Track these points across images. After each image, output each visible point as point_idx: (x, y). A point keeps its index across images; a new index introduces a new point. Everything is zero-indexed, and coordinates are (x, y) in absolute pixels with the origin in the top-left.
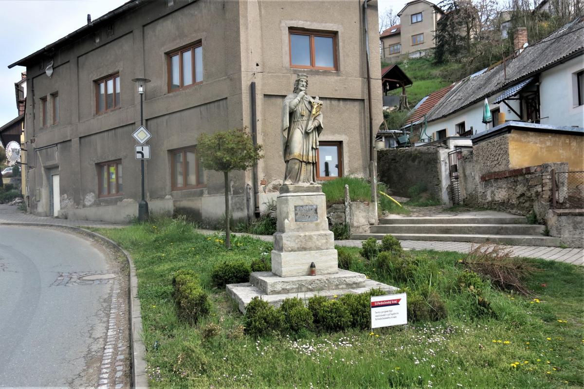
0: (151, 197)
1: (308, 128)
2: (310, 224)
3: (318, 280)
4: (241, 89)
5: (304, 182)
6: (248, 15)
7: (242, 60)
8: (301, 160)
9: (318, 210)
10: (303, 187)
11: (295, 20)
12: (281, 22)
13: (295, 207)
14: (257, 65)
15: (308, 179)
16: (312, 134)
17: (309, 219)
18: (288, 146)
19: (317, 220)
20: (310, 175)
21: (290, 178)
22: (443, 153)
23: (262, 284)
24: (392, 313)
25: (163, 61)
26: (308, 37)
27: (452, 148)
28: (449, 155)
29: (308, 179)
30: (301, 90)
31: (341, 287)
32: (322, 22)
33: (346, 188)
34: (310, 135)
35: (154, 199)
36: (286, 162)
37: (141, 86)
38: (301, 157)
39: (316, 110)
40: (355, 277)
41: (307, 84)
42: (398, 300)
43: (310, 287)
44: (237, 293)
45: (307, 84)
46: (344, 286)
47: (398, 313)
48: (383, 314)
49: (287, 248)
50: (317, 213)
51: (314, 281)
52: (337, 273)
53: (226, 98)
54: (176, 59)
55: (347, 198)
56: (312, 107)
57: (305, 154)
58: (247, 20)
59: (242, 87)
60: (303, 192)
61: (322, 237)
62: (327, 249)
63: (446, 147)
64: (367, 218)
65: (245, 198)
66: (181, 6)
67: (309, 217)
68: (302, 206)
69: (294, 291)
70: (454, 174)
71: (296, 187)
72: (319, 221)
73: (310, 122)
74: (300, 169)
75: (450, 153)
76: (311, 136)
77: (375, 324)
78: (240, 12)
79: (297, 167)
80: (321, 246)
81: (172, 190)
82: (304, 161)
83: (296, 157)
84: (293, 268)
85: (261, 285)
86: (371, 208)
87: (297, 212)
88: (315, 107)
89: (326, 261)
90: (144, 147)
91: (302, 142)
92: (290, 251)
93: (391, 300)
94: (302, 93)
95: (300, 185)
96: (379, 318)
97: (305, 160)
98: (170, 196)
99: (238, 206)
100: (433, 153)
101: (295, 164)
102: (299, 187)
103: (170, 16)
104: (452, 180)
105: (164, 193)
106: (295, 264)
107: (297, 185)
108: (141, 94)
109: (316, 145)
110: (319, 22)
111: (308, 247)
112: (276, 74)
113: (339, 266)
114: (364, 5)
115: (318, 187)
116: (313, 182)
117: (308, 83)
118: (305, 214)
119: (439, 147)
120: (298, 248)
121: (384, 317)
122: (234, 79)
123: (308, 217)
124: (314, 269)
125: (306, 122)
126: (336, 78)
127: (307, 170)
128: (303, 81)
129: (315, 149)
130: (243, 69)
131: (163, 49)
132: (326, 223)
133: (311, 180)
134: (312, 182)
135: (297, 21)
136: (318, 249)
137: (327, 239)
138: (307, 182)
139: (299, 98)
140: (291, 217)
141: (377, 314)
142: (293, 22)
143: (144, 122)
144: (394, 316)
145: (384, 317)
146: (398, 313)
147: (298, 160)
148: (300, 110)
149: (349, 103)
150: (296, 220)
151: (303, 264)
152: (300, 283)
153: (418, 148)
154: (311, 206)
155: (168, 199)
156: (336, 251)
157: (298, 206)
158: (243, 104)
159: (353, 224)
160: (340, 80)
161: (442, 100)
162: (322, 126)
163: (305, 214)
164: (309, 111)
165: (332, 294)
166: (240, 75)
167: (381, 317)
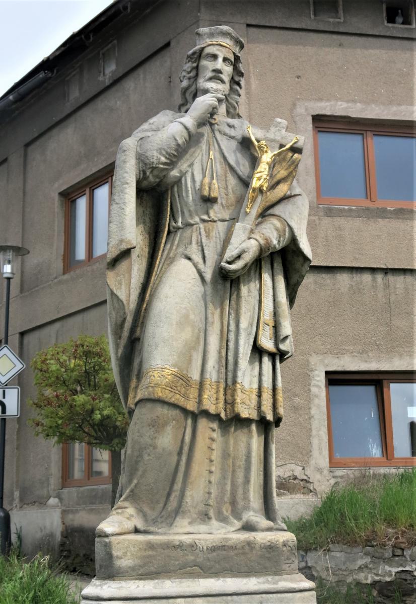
0: (22, 500)
5: (205, 517)
8: (191, 406)
10: (193, 546)
11: (328, 100)
12: (294, 105)
15: (233, 503)
16: (254, 285)
18: (138, 339)
20: (247, 481)
21: (134, 497)
25: (56, 210)
26: (359, 138)
30: (206, 91)
32: (391, 103)
34: (244, 290)
35: (28, 504)
36: (39, 422)
37: (9, 262)
38: (193, 393)
39: (271, 176)
41: (237, 72)
45: (237, 72)
54: (82, 204)
56: (254, 162)
60: (191, 575)
66: (92, 95)
71: (151, 546)
74: (186, 452)
76: (248, 291)
79: (167, 440)
81: (63, 486)
82: (206, 413)
83: (159, 393)
88: (267, 158)
90: (6, 390)
91: (196, 317)
97: (210, 405)
98: (56, 500)
101: (157, 425)
102: (168, 546)
103: (72, 119)
105: (45, 492)
108: (9, 279)
110: (383, 104)
117: (241, 67)
125: (221, 227)
127: (225, 455)
128: (215, 57)
131: (56, 185)
133: (247, 508)
135: (332, 103)
142: (323, 104)
143: (14, 339)
147: (175, 406)
148: (198, 178)
155: (54, 507)
162: (305, 246)
164: (240, 179)
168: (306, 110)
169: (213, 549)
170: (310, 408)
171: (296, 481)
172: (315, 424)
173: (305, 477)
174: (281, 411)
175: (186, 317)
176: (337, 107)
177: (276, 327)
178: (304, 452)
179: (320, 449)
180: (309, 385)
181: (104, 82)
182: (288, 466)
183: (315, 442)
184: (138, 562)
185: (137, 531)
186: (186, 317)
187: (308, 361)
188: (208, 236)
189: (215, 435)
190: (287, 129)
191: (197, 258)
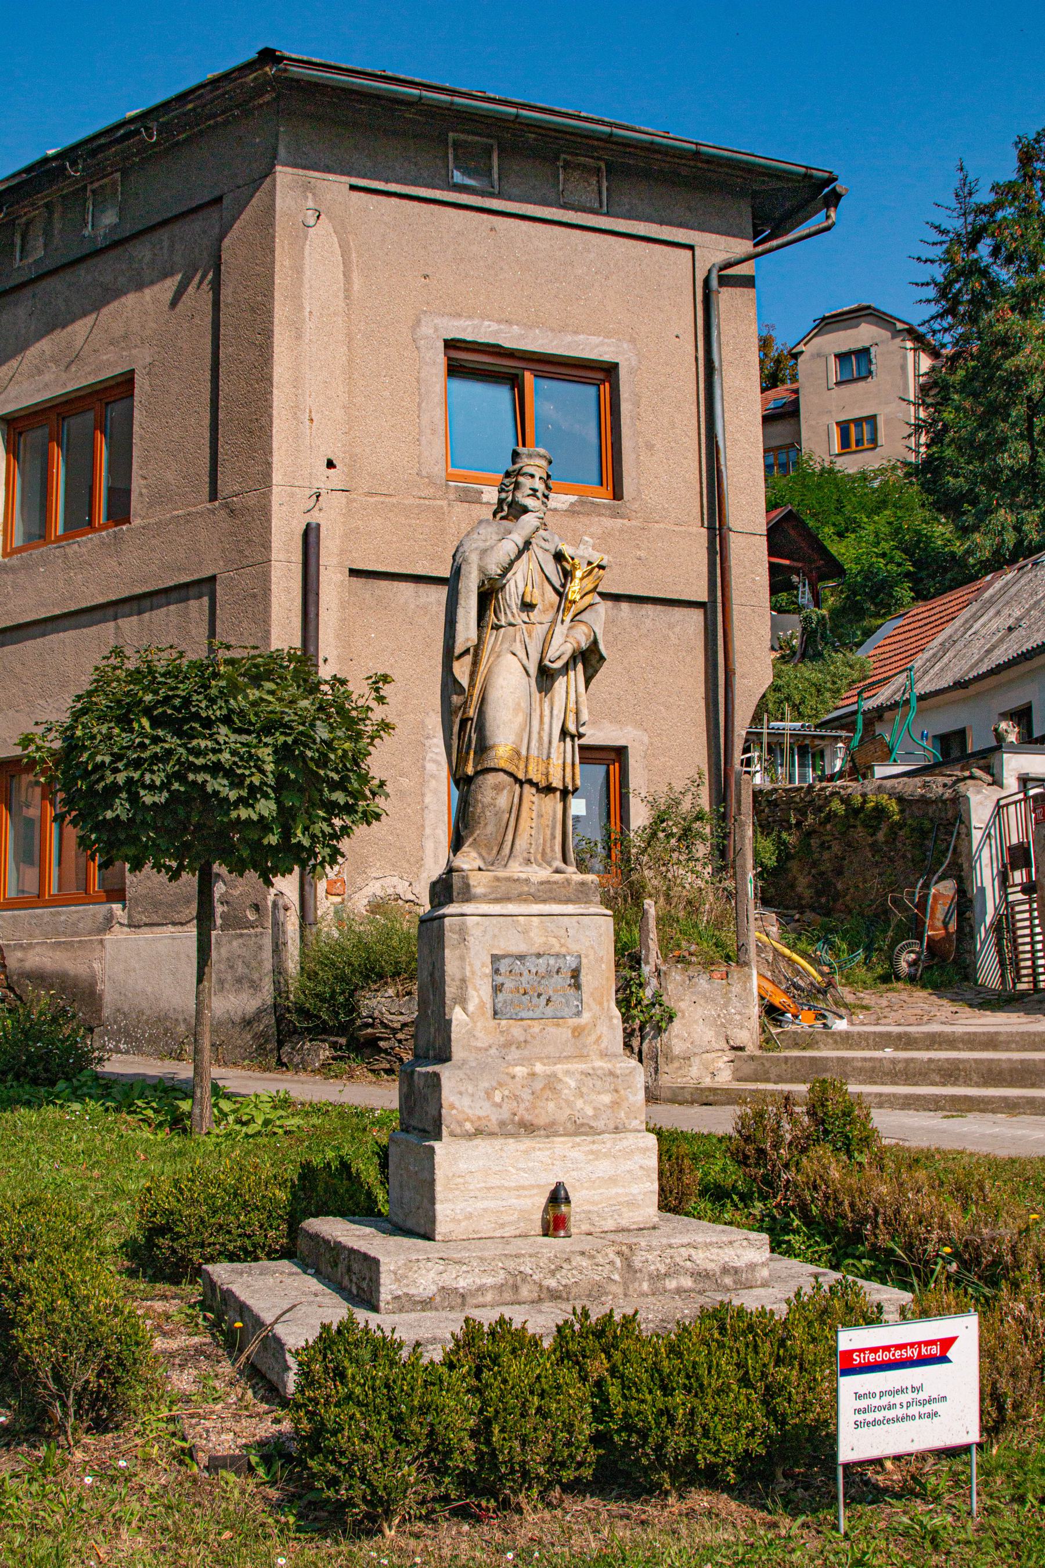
1: (551, 654)
2: (551, 1029)
3: (583, 1253)
4: (267, 546)
6: (306, 290)
7: (275, 445)
9: (583, 973)
10: (527, 881)
12: (418, 322)
13: (495, 958)
14: (330, 464)
15: (544, 853)
17: (549, 1011)
19: (579, 1014)
22: (980, 803)
23: (356, 1267)
24: (922, 1396)
27: (1011, 783)
28: (999, 808)
29: (544, 853)
31: (671, 1284)
32: (563, 329)
33: (645, 913)
38: (522, 766)
40: (731, 1243)
42: (947, 1343)
43: (552, 1283)
44: (250, 1302)
46: (687, 1282)
47: (944, 1398)
48: (886, 1400)
49: (460, 1124)
50: (577, 986)
51: (568, 1260)
52: (654, 1228)
53: (213, 579)
55: (648, 949)
57: (534, 752)
58: (300, 308)
59: (274, 538)
61: (599, 1083)
62: (617, 1130)
63: (989, 779)
64: (722, 1027)
65: (267, 942)
67: (549, 1000)
68: (521, 957)
69: (489, 1297)
70: (1018, 876)
72: (586, 1016)
73: (560, 630)
75: (1002, 802)
76: (560, 683)
77: (854, 1444)
78: (277, 281)
79: (503, 801)
80: (595, 1117)
82: (530, 782)
83: (502, 764)
84: (480, 1205)
85: (349, 1270)
86: (736, 989)
87: (499, 979)
89: (613, 1180)
91: (524, 704)
92: (470, 1136)
93: (919, 1343)
94: (529, 521)
95: (516, 876)
96: (870, 1417)
99: (241, 969)
100: (944, 802)
101: (498, 788)
102: (508, 879)
104: (1011, 898)
106: (488, 1189)
107: (502, 874)
109: (578, 724)
111: (541, 1121)
112: (394, 500)
113: (664, 1206)
114: (707, 281)
115: (583, 883)
116: (563, 866)
118: (530, 987)
119: (965, 779)
120: (502, 1124)
121: (890, 1414)
122: (250, 521)
123: (543, 1000)
124: (564, 1208)
126: (608, 522)
128: (532, 476)
129: (572, 737)
130: (277, 477)
132: (611, 1027)
133: (554, 859)
134: (558, 863)
136: (580, 1129)
137: (616, 1091)
138: (539, 865)
139: (517, 539)
140: (476, 1000)
141: (863, 1403)
144: (928, 1408)
145: (890, 1414)
146: (944, 1398)
147: (511, 774)
149: (649, 609)
150: (495, 1013)
151: (523, 1188)
152: (511, 1265)
153: (888, 783)
154: (557, 955)
156: (652, 1140)
157: (504, 956)
158: (273, 599)
159: (669, 1047)
160: (621, 531)
161: (949, 630)
163: (530, 987)
165: (658, 1310)
166: (267, 496)
167: (879, 1415)
168: (436, 330)
169: (542, 883)
170: (423, 795)
171: (400, 902)
172: (430, 817)
173: (413, 898)
174: (578, 782)
175: (519, 704)
176: (483, 330)
177: (577, 714)
178: (412, 860)
179: (436, 856)
180: (424, 759)
181: (93, 239)
182: (388, 880)
183: (429, 845)
184: (488, 890)
185: (480, 869)
186: (519, 704)
187: (423, 722)
188: (530, 636)
189: (534, 799)
190: (594, 548)
191: (522, 654)
